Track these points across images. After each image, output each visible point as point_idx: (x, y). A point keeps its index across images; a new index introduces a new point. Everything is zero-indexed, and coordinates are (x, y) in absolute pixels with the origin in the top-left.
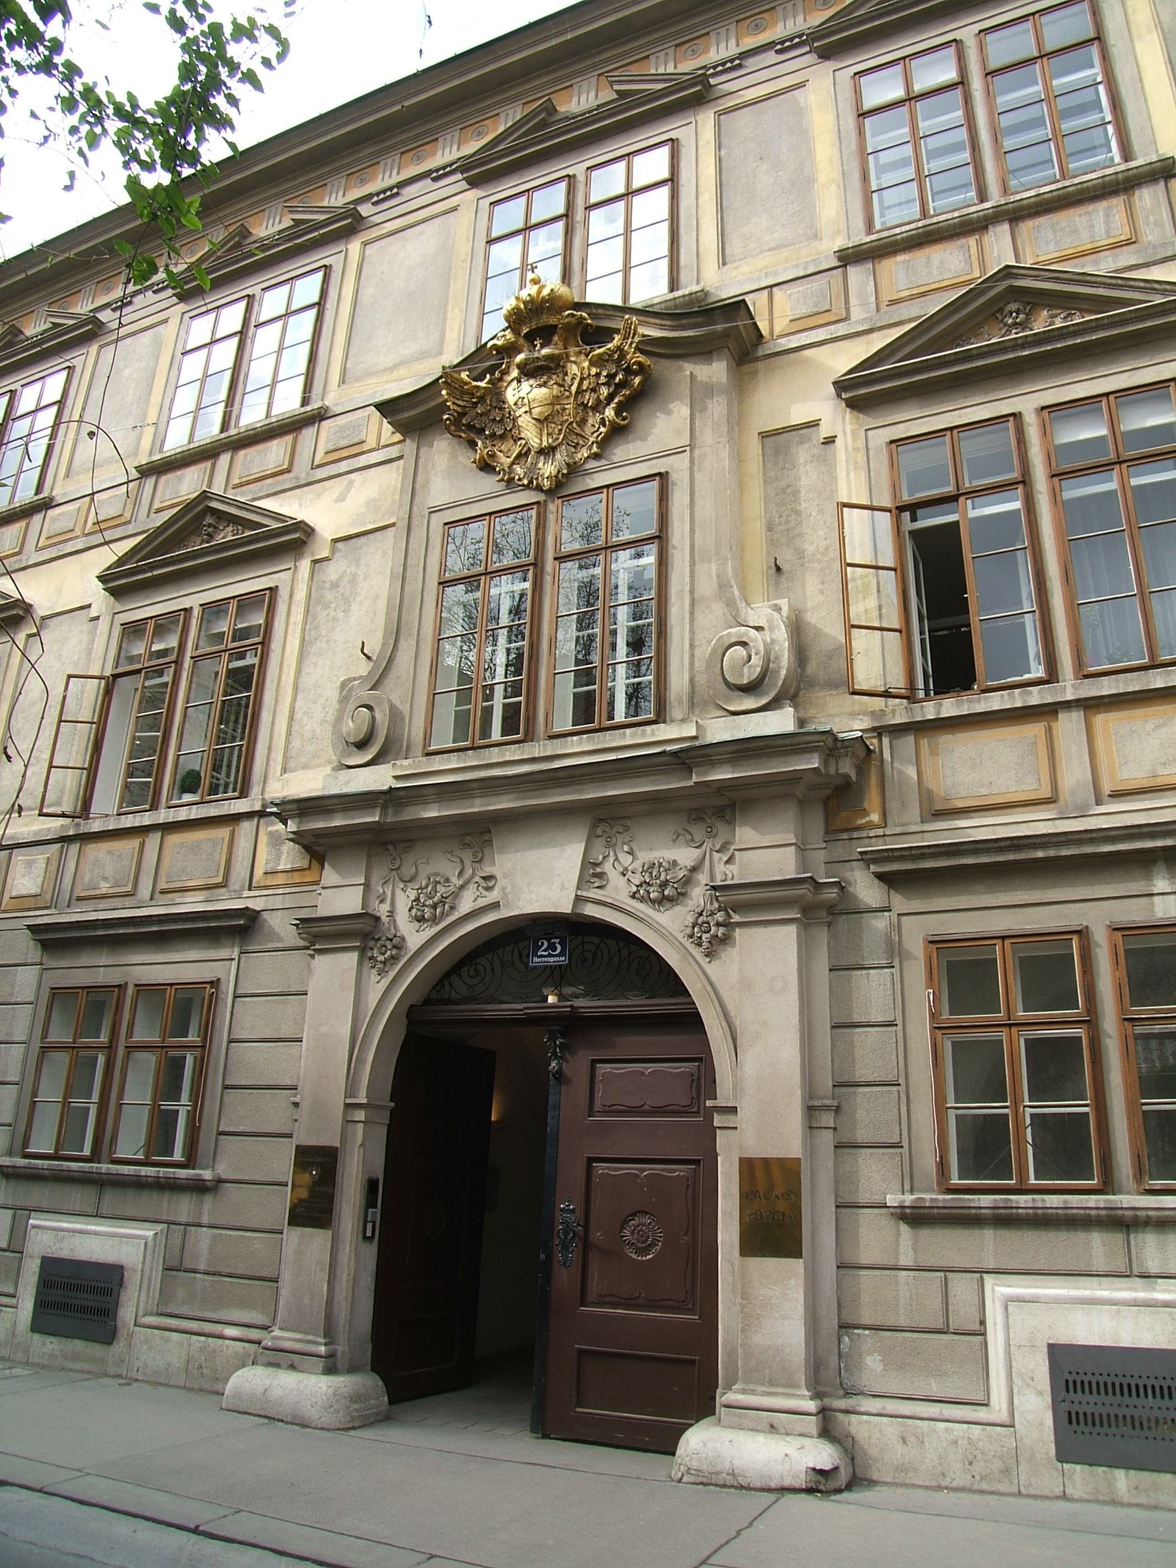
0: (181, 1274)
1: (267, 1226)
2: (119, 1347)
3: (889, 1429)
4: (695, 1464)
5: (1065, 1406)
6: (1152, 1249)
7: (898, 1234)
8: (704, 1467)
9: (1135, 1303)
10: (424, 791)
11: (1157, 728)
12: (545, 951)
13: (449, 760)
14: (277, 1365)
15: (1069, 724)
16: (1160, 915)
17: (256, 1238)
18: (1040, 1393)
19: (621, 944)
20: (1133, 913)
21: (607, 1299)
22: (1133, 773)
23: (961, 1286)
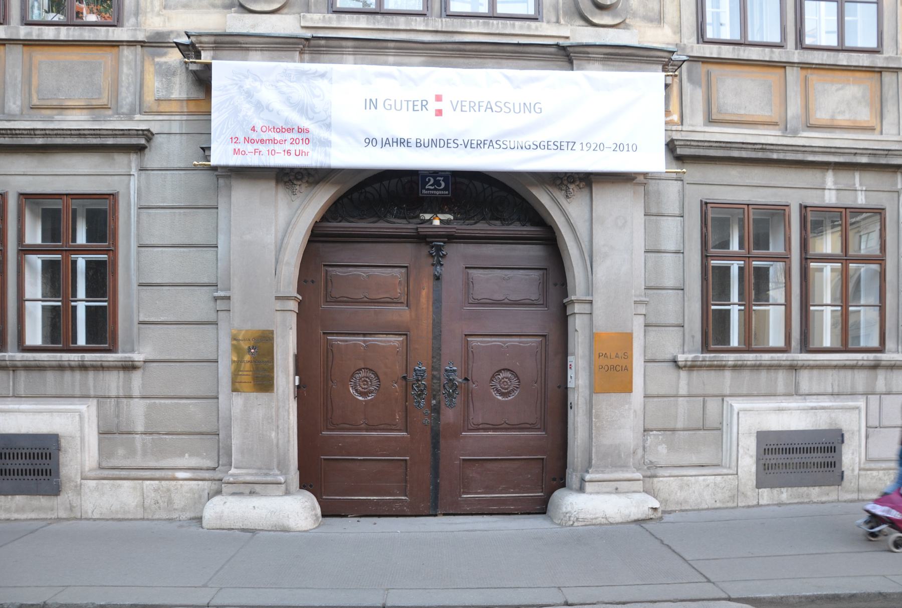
0: (117, 436)
1: (200, 394)
2: (67, 496)
3: (674, 483)
4: (581, 516)
5: (763, 462)
6: (806, 380)
7: (679, 377)
8: (589, 516)
9: (798, 409)
10: (344, 43)
11: (837, 90)
12: (431, 185)
13: (358, 20)
14: (240, 494)
15: (793, 74)
16: (827, 201)
17: (189, 404)
18: (751, 457)
19: (486, 186)
20: (812, 199)
21: (481, 426)
22: (821, 115)
23: (713, 405)
